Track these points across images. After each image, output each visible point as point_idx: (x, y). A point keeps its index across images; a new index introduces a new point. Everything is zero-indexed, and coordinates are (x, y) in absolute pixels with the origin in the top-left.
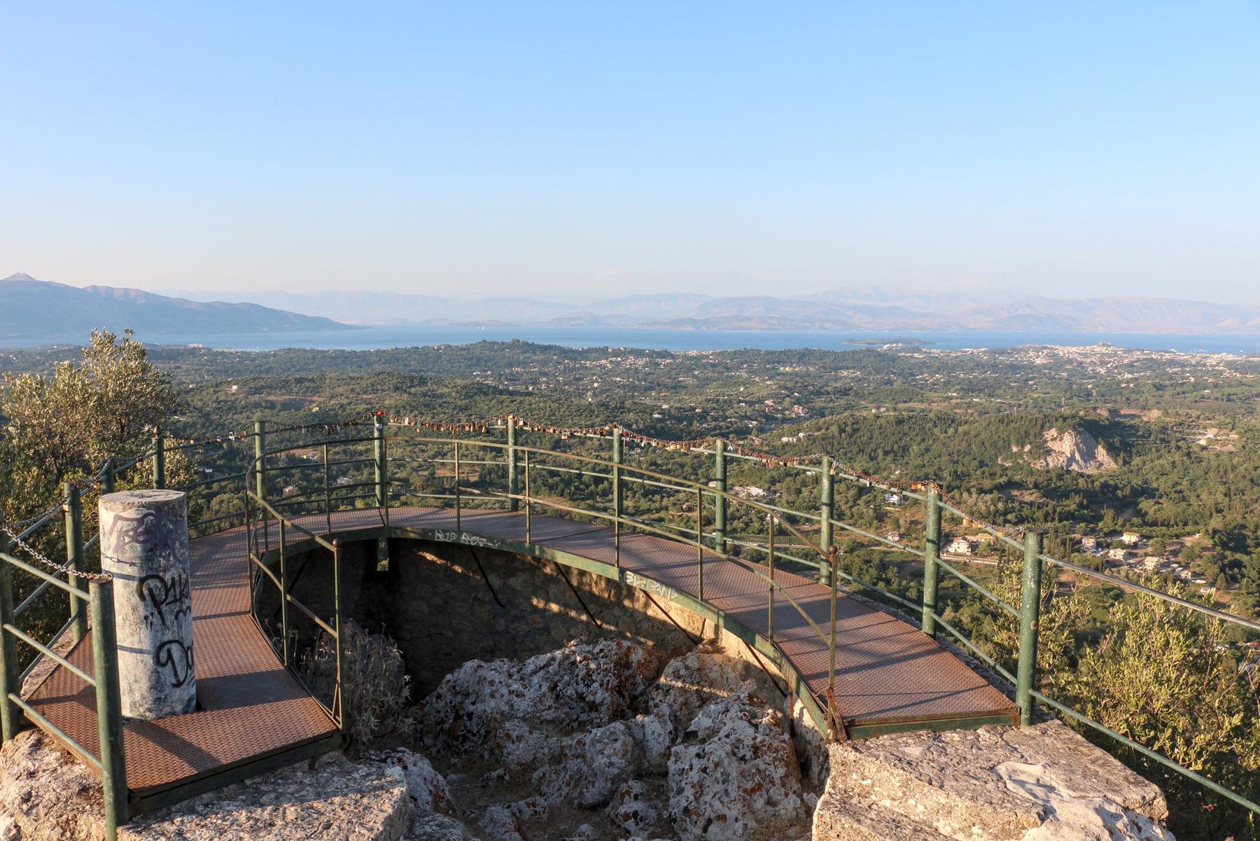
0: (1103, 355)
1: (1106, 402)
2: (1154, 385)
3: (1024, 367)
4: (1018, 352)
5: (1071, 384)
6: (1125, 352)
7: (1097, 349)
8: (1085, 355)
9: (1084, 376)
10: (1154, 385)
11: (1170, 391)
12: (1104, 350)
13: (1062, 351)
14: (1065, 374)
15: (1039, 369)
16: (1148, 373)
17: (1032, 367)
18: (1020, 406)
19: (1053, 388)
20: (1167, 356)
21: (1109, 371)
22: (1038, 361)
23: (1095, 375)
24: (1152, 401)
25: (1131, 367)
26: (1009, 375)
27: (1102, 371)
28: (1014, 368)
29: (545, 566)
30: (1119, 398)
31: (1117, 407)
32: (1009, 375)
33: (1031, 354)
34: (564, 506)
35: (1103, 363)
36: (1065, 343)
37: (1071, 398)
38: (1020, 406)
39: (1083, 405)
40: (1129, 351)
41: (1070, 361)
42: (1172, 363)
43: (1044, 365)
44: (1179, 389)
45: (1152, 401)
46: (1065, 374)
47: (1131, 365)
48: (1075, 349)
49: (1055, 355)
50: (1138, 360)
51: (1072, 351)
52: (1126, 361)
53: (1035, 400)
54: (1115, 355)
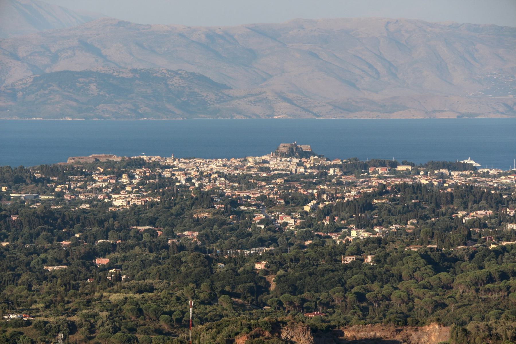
0: (291, 179)
1: (303, 307)
2: (425, 256)
3: (81, 220)
4: (64, 174)
5: (210, 262)
6: (346, 170)
7: (276, 164)
8: (245, 181)
9: (245, 237)
10: (425, 256)
11: (469, 273)
12: (293, 165)
13: (181, 170)
14: (192, 236)
15: (122, 221)
16: (411, 225)
17: (104, 219)
18: (73, 328)
19: (163, 276)
20: (456, 177)
21: (308, 222)
22: (119, 202)
23: (274, 234)
24: (423, 300)
25: (363, 210)
26: (41, 243)
27: (291, 222)
28: (55, 222)
29: (433, 185)
30: (337, 296)
31: (334, 319)
32: (41, 243)
33: (100, 180)
34: (203, 116)
35: (293, 203)
36: (189, 150)
37: (212, 300)
38: (73, 328)
39: (244, 318)
40: (356, 167)
41: (206, 199)
42: (470, 196)
43: (136, 211)
44: (491, 267)
45: (423, 300)
46: (192, 236)
47: (364, 205)
48: (216, 165)
49: (165, 182)
50: (382, 191)
51: (213, 170)
52: (352, 194)
53: (115, 310)
54: (323, 175)
